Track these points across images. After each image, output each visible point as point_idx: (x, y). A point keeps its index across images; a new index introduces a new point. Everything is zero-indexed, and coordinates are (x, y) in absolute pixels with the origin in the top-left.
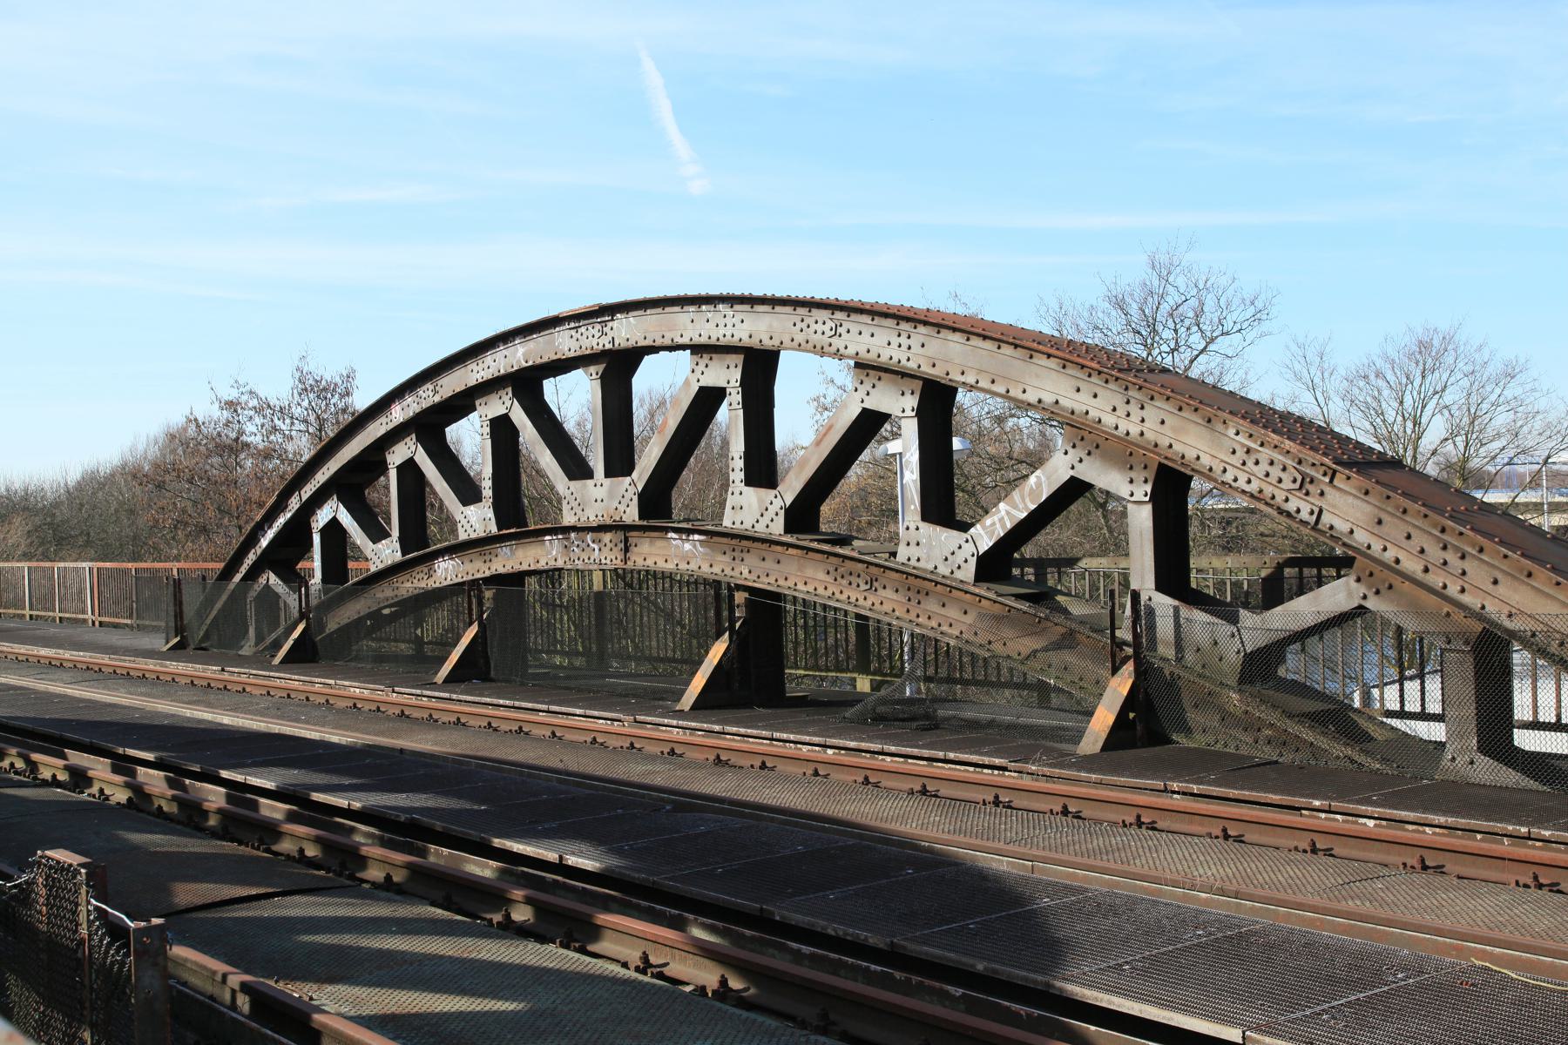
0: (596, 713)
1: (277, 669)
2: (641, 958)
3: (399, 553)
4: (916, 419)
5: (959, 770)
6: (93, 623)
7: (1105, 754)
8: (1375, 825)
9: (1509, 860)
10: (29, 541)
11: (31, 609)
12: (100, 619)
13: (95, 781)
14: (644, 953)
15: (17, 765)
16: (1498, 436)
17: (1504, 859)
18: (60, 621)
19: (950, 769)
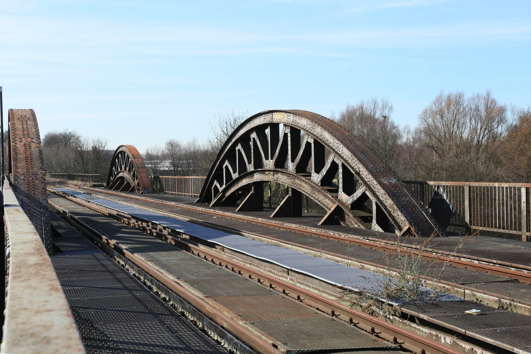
0: (521, 266)
1: (210, 208)
2: (349, 320)
3: (253, 169)
4: (5, 203)
5: (483, 264)
6: (192, 196)
7: (322, 226)
8: (528, 272)
9: (455, 262)
10: (132, 173)
11: (178, 192)
12: (194, 194)
13: (168, 239)
14: (351, 318)
15: (172, 243)
16: (457, 131)
17: (509, 273)
18: (184, 196)
19: (484, 264)
